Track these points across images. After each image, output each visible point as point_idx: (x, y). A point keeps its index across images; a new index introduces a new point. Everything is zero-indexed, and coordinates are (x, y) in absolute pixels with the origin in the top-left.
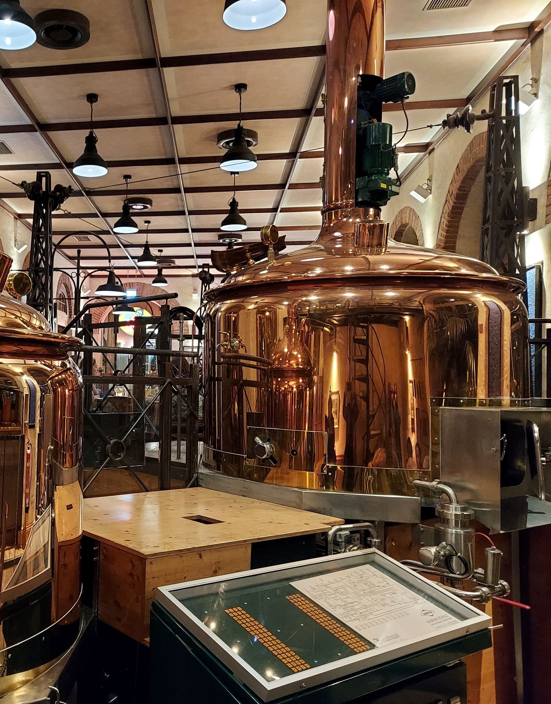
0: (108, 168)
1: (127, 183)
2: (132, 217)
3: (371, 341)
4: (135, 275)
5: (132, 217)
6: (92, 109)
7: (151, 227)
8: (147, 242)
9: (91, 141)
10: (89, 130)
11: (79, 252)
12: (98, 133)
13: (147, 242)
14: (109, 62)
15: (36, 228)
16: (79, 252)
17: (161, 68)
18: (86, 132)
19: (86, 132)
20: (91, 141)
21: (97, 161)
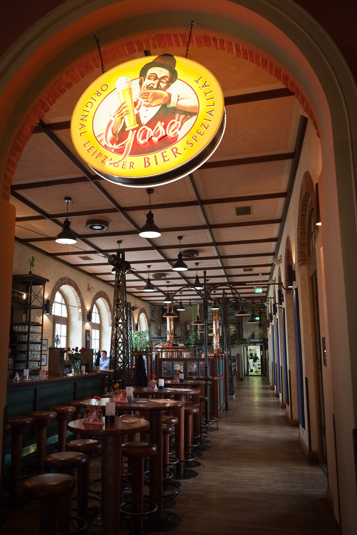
0: (161, 233)
1: (61, 336)
2: (184, 262)
3: (259, 303)
4: (253, 274)
5: (184, 262)
6: (150, 200)
7: (170, 284)
8: (197, 275)
9: (150, 217)
10: (149, 210)
11: (205, 273)
12: (154, 212)
13: (197, 275)
14: (262, 92)
15: (117, 281)
16: (205, 273)
17: (44, 311)
18: (147, 212)
19: (147, 212)
20: (150, 217)
21: (155, 229)
